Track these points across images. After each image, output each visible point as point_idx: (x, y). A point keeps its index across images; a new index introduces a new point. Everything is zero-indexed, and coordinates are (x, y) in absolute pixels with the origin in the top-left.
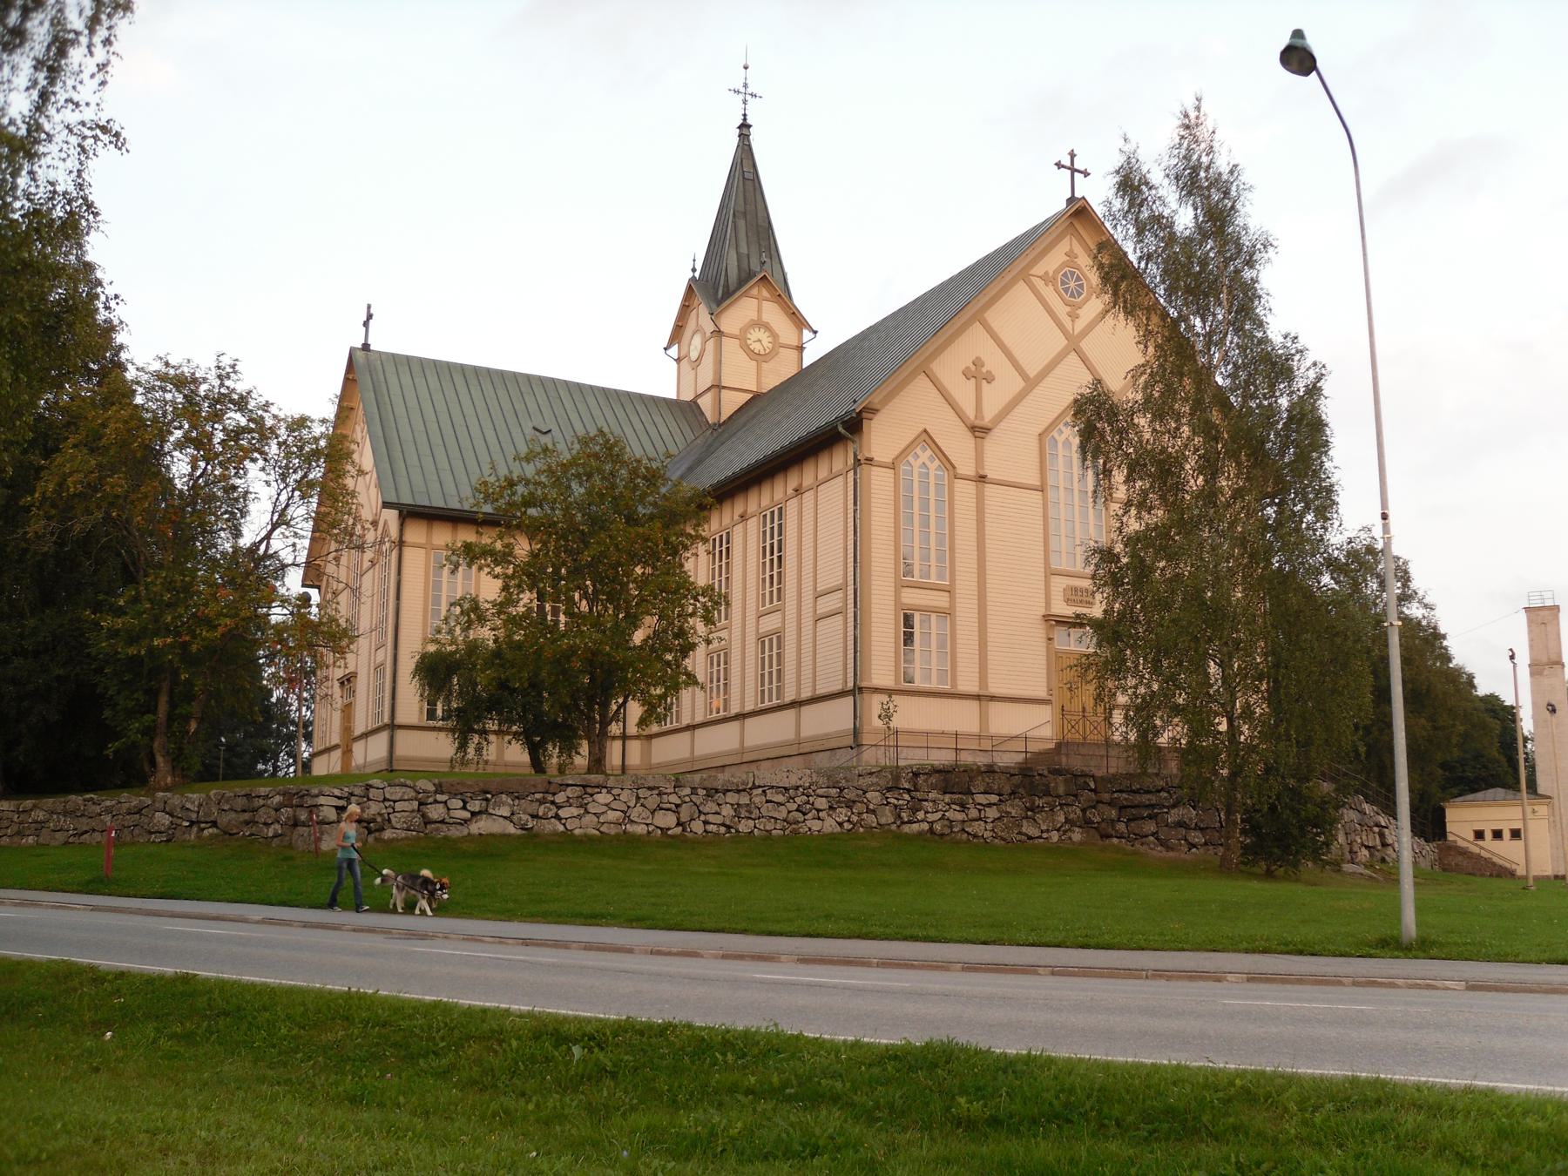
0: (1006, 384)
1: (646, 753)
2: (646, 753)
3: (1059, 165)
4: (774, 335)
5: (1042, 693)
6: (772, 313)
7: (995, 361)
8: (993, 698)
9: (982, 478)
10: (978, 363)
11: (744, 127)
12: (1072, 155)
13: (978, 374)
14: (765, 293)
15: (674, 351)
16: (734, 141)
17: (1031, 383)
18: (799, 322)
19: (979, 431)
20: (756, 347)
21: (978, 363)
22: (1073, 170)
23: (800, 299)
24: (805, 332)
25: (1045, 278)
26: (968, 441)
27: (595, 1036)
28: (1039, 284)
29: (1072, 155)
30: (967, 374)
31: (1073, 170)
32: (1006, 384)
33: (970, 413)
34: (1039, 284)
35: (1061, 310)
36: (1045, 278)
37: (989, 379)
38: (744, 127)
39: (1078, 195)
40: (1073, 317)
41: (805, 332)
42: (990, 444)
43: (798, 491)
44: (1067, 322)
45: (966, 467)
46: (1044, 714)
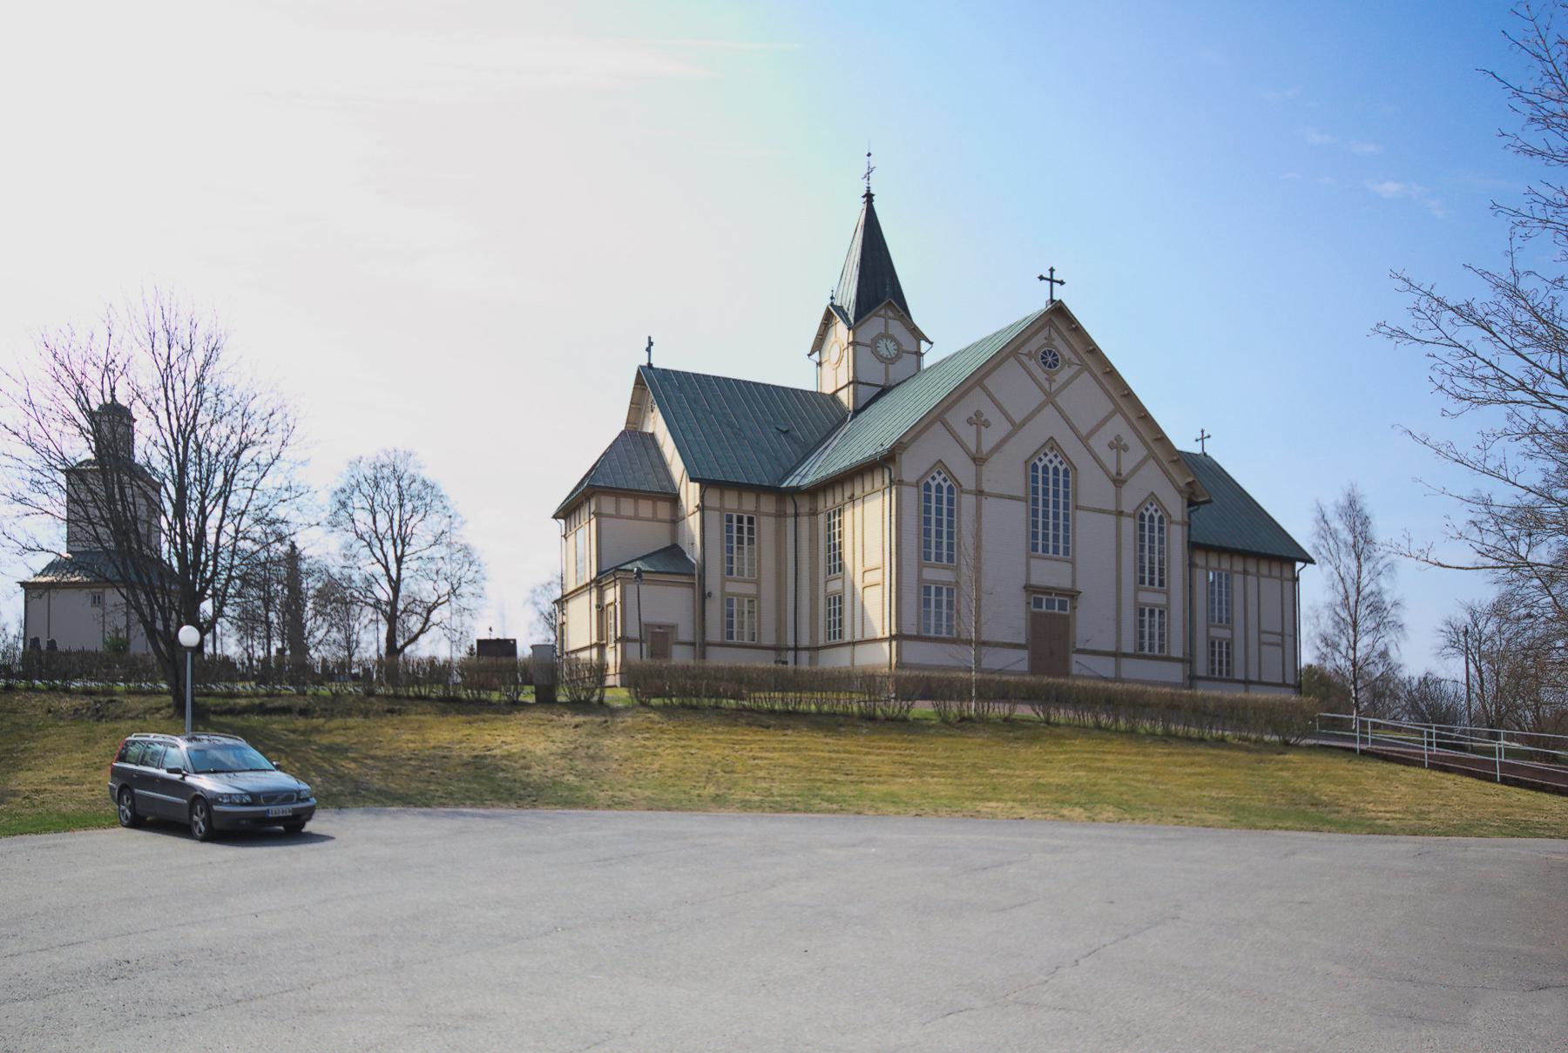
0: (998, 429)
1: (812, 661)
2: (812, 661)
3: (1041, 278)
4: (898, 344)
5: (1023, 641)
6: (896, 328)
7: (990, 413)
8: (985, 644)
9: (980, 493)
10: (978, 414)
11: (869, 197)
12: (1052, 270)
13: (978, 421)
14: (891, 314)
15: (816, 356)
16: (861, 206)
17: (1016, 427)
18: (918, 335)
19: (978, 460)
20: (885, 353)
21: (978, 414)
22: (1052, 280)
23: (917, 319)
24: (923, 343)
25: (1029, 355)
26: (972, 467)
27: (47, 830)
28: (1024, 359)
29: (1052, 270)
30: (970, 422)
31: (1052, 280)
32: (999, 428)
33: (973, 450)
34: (1024, 359)
35: (1041, 376)
36: (1029, 355)
37: (987, 424)
38: (869, 197)
39: (1056, 298)
40: (1050, 381)
41: (923, 343)
42: (986, 470)
43: (852, 499)
44: (1046, 385)
45: (969, 483)
46: (1024, 654)
